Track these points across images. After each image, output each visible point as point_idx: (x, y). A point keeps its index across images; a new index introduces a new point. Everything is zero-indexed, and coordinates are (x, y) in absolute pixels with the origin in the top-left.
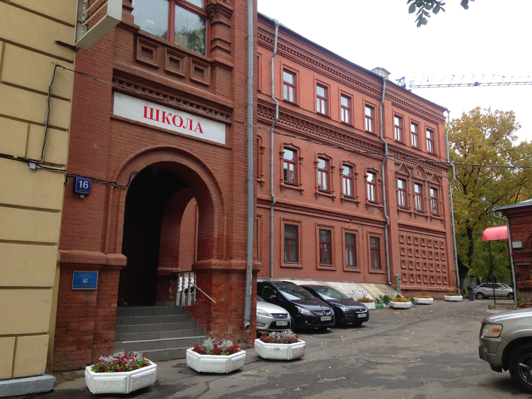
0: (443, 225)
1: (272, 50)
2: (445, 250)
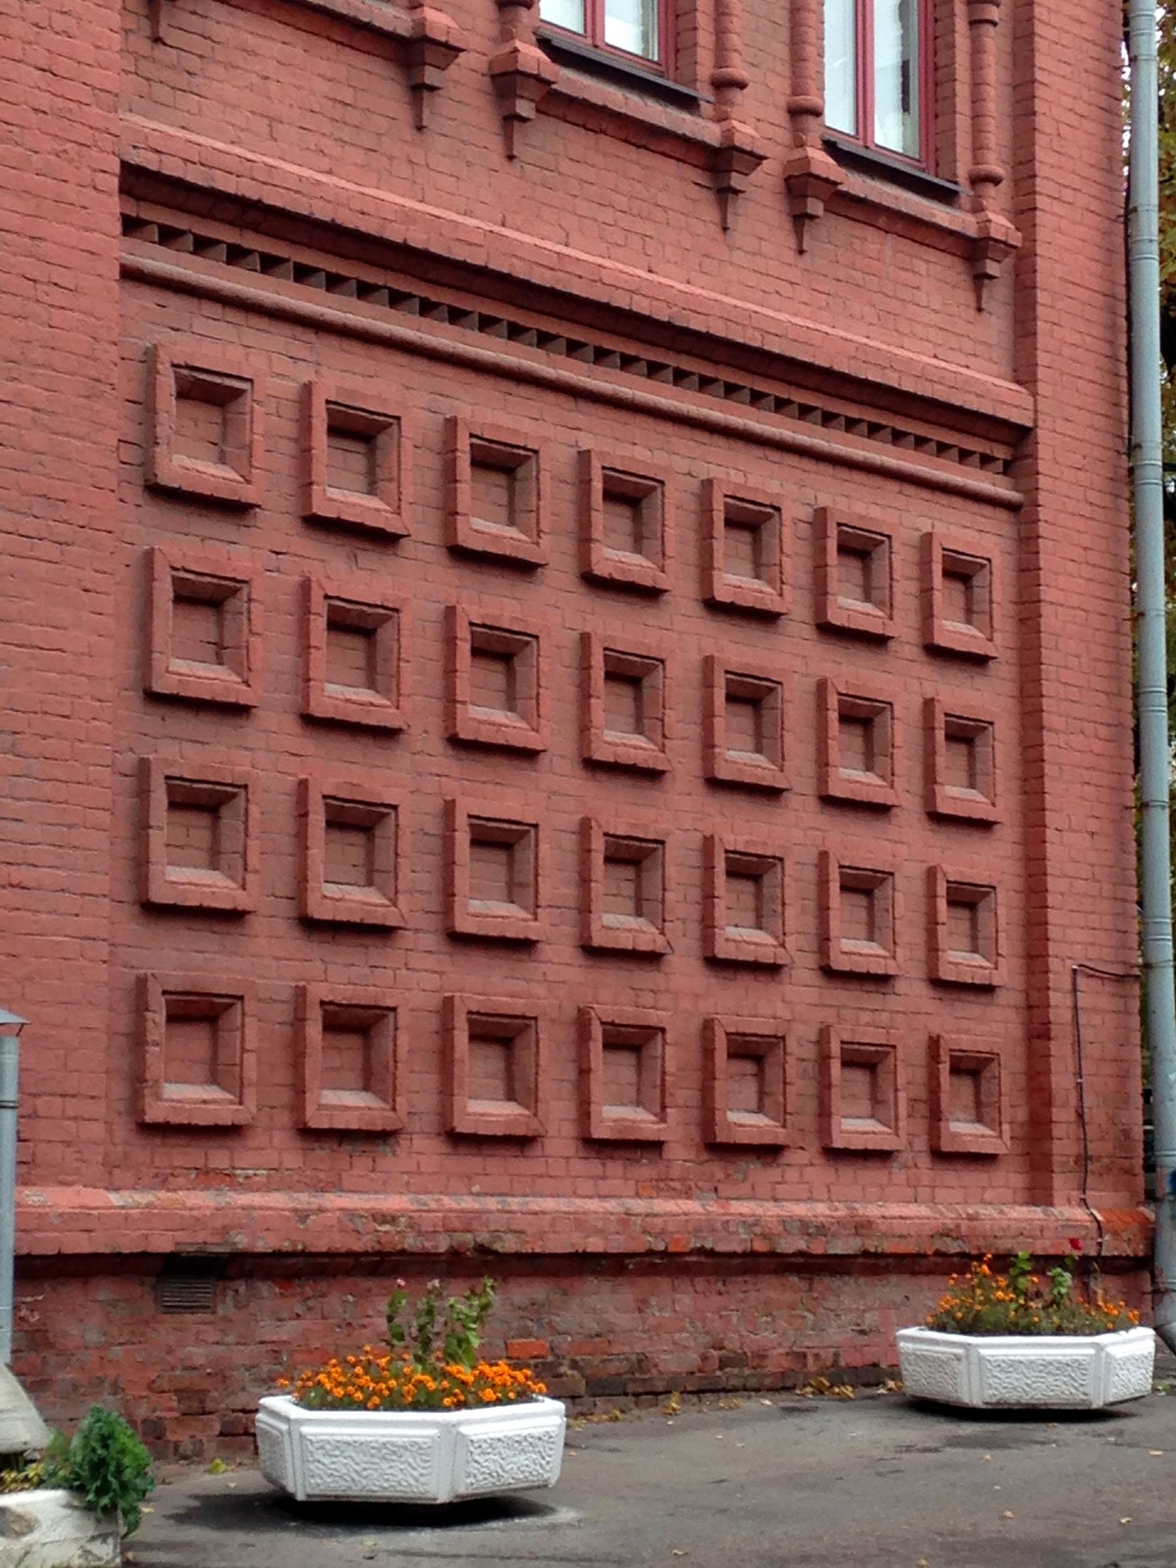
2: (1003, 672)
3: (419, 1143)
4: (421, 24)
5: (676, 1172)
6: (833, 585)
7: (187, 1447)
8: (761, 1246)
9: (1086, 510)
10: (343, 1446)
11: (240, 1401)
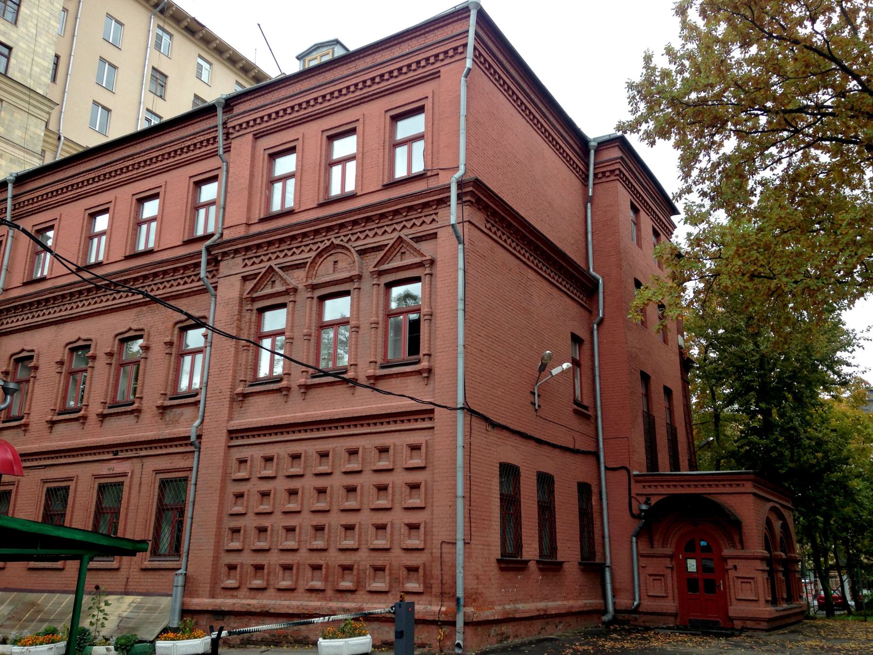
3: (272, 590)
5: (328, 596)
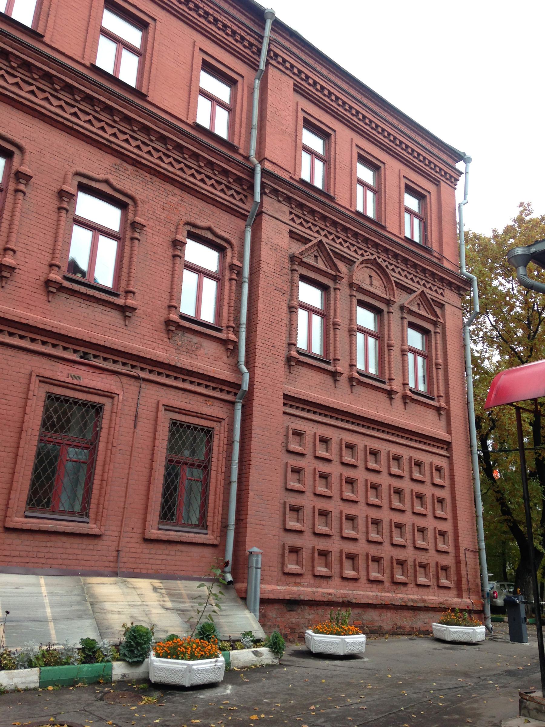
0: (443, 423)
1: (297, 88)
4: (336, 369)
5: (386, 587)
6: (413, 471)
7: (292, 640)
8: (404, 604)
9: (463, 458)
10: (322, 642)
11: (302, 631)
